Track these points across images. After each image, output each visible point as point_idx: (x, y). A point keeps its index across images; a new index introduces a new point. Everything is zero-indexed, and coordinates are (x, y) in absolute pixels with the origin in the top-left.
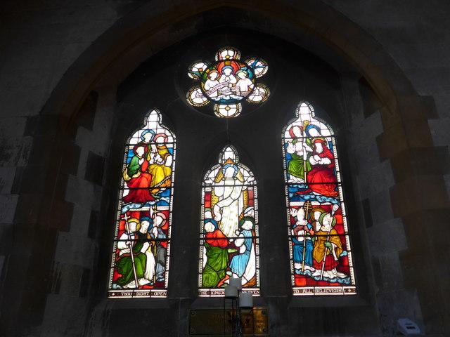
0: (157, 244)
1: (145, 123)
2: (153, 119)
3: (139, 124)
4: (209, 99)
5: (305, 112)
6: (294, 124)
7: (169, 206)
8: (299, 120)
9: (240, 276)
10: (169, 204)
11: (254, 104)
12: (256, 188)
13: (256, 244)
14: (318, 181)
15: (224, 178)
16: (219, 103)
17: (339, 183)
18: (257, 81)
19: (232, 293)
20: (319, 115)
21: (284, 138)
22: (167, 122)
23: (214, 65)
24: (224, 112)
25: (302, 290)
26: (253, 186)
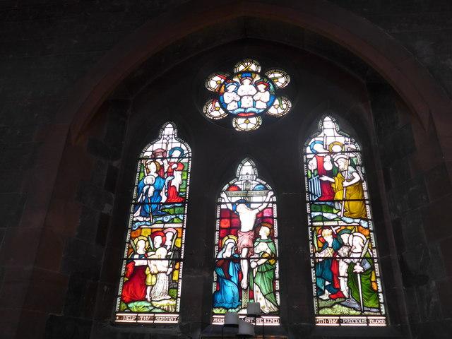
0: (361, 166)
1: (160, 137)
2: (169, 130)
3: (154, 136)
4: (226, 111)
5: (329, 125)
6: (317, 139)
7: (183, 223)
8: (322, 134)
9: (320, 300)
10: (183, 221)
11: (274, 117)
12: (275, 206)
13: (372, 248)
14: (351, 202)
15: (155, 250)
16: (237, 116)
17: (276, 238)
18: (278, 93)
19: (232, 321)
20: (342, 131)
21: (306, 154)
22: (182, 135)
23: (217, 96)
24: (242, 125)
25: (122, 317)
26: (273, 203)
